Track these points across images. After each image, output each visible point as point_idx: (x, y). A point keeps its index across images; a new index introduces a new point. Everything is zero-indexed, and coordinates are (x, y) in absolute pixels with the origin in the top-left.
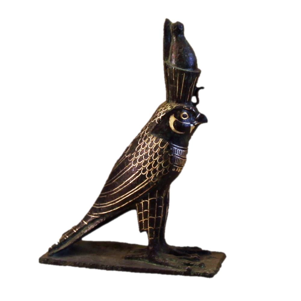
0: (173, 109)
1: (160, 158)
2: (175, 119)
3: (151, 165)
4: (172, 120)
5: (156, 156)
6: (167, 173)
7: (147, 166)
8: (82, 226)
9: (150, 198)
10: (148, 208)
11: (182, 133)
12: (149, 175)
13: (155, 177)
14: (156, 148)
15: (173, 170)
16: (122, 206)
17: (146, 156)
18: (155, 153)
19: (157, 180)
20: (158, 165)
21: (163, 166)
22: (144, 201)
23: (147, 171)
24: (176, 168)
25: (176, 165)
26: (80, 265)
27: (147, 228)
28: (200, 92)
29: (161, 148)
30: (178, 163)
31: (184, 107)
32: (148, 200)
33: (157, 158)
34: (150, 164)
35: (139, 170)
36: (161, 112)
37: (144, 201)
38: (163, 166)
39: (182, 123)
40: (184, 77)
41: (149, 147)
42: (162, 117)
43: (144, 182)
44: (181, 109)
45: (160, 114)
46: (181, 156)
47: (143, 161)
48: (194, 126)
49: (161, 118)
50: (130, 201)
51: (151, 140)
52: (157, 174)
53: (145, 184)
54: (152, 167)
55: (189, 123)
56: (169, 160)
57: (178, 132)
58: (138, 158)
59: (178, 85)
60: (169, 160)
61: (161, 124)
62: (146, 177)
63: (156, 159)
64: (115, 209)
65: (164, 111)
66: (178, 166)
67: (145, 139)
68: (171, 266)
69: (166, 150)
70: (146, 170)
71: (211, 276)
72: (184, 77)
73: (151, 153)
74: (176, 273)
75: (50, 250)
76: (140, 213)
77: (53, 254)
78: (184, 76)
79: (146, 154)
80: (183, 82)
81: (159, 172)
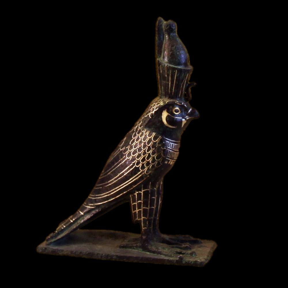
0: (165, 104)
1: (153, 151)
2: (168, 114)
3: (144, 158)
4: (165, 115)
5: (149, 149)
6: (160, 165)
7: (140, 159)
8: (79, 217)
9: (143, 190)
10: (142, 199)
11: (174, 127)
12: (143, 167)
13: (148, 169)
14: (149, 142)
15: (165, 162)
16: (117, 197)
17: (140, 149)
18: (148, 146)
19: (150, 172)
20: (151, 158)
21: (156, 159)
22: (137, 192)
23: (141, 164)
24: (169, 161)
25: (168, 158)
27: (141, 218)
29: (154, 142)
30: (170, 156)
31: (176, 103)
32: (141, 191)
33: (151, 151)
34: (144, 157)
35: (133, 162)
36: (154, 108)
37: (137, 192)
38: (156, 159)
39: (174, 118)
40: (176, 74)
41: (143, 141)
42: (155, 112)
43: (137, 174)
45: (153, 109)
46: (173, 150)
47: (137, 154)
48: (186, 121)
49: (154, 113)
50: (125, 193)
51: (144, 134)
52: (150, 167)
53: (139, 176)
54: (145, 160)
55: (181, 118)
56: (162, 153)
57: (170, 126)
58: (132, 151)
59: (170, 81)
60: (162, 153)
63: (149, 152)
64: (110, 200)
65: (157, 106)
66: (170, 159)
67: (138, 133)
68: (164, 255)
69: (159, 144)
70: (140, 163)
72: (176, 74)
73: (145, 146)
76: (134, 203)
77: (51, 243)
78: (176, 73)
79: (140, 147)
80: (175, 78)
81: (153, 165)
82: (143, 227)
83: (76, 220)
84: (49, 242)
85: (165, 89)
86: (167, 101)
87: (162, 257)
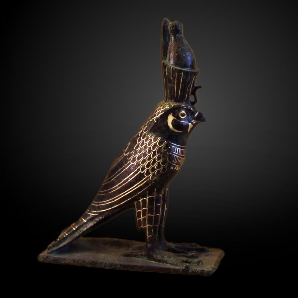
0: (171, 107)
1: (158, 156)
2: (174, 118)
3: (149, 163)
4: (170, 118)
5: (154, 154)
6: (166, 171)
7: (145, 164)
8: (81, 224)
9: (148, 196)
10: (147, 206)
11: (180, 132)
12: (148, 173)
13: (154, 175)
14: (154, 147)
15: (171, 168)
16: (121, 204)
17: (145, 155)
18: (153, 151)
19: (155, 178)
20: (156, 163)
21: (161, 164)
22: (142, 199)
23: (145, 169)
24: (174, 166)
25: (174, 163)
27: (146, 225)
28: (197, 92)
29: (159, 147)
30: (176, 161)
31: (182, 106)
32: (146, 198)
33: (156, 156)
34: (149, 163)
35: (137, 168)
36: (159, 111)
37: (142, 199)
38: (161, 164)
39: (180, 122)
40: (182, 77)
41: (148, 146)
42: (161, 116)
43: (142, 181)
44: (179, 108)
45: (159, 113)
46: (179, 155)
47: (141, 160)
48: (192, 125)
49: (159, 117)
50: (129, 199)
51: (149, 139)
52: (156, 173)
53: (144, 183)
54: (150, 165)
55: (187, 122)
56: (168, 158)
57: (176, 131)
58: (136, 156)
59: (176, 84)
60: (168, 158)
62: (144, 175)
63: (155, 157)
64: (114, 207)
65: (162, 110)
66: (176, 164)
67: (143, 138)
68: (170, 264)
69: (164, 149)
70: (145, 168)
72: (182, 77)
73: (150, 151)
76: (139, 210)
77: (53, 251)
78: (182, 75)
79: (144, 152)
80: (181, 81)
81: (158, 171)
82: (148, 235)
83: (79, 228)
84: (51, 250)
85: (171, 92)
86: (173, 104)
87: (168, 266)
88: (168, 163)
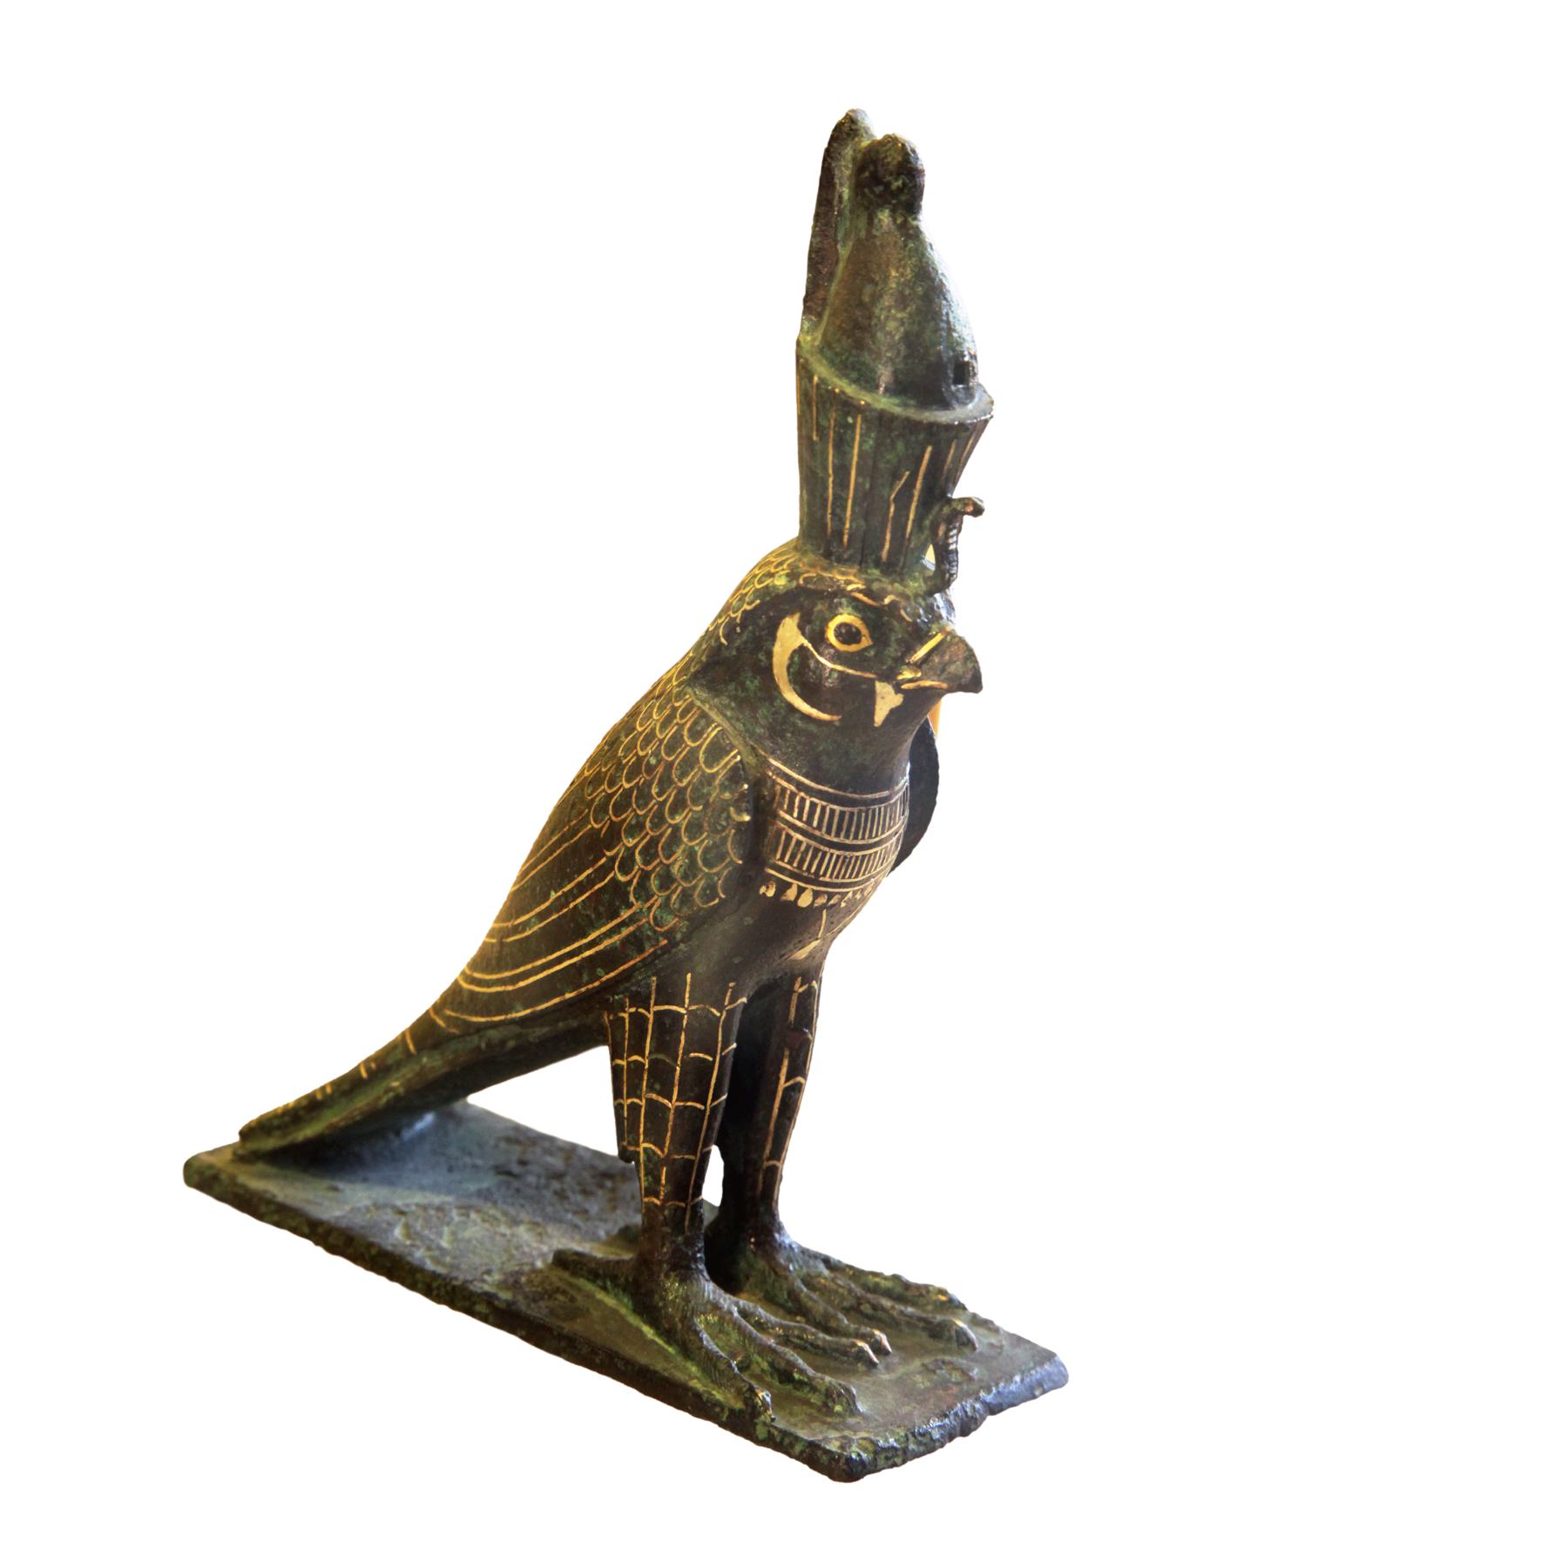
3: (653, 842)
6: (716, 901)
10: (647, 1052)
13: (666, 905)
15: (763, 890)
24: (783, 887)
25: (781, 870)
26: (331, 1240)
30: (790, 862)
35: (608, 854)
46: (817, 833)
49: (738, 621)
50: (568, 996)
55: (872, 676)
56: (730, 839)
57: (805, 707)
60: (730, 839)
61: (738, 649)
62: (697, 863)
65: (758, 587)
66: (792, 875)
69: (723, 787)
71: (845, 1470)
74: (700, 1407)
75: (247, 1133)
78: (858, 431)
80: (852, 459)
88: (732, 861)
